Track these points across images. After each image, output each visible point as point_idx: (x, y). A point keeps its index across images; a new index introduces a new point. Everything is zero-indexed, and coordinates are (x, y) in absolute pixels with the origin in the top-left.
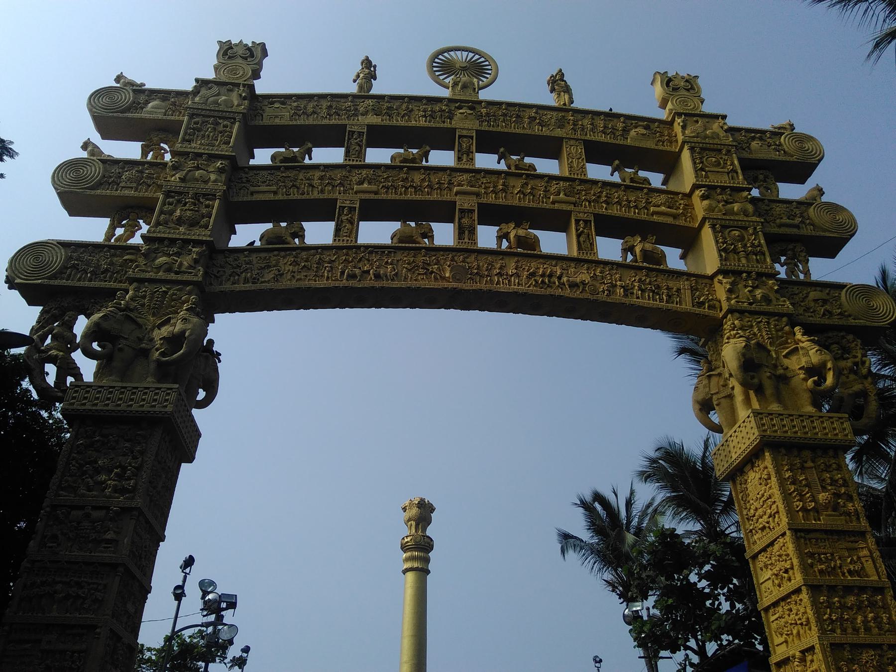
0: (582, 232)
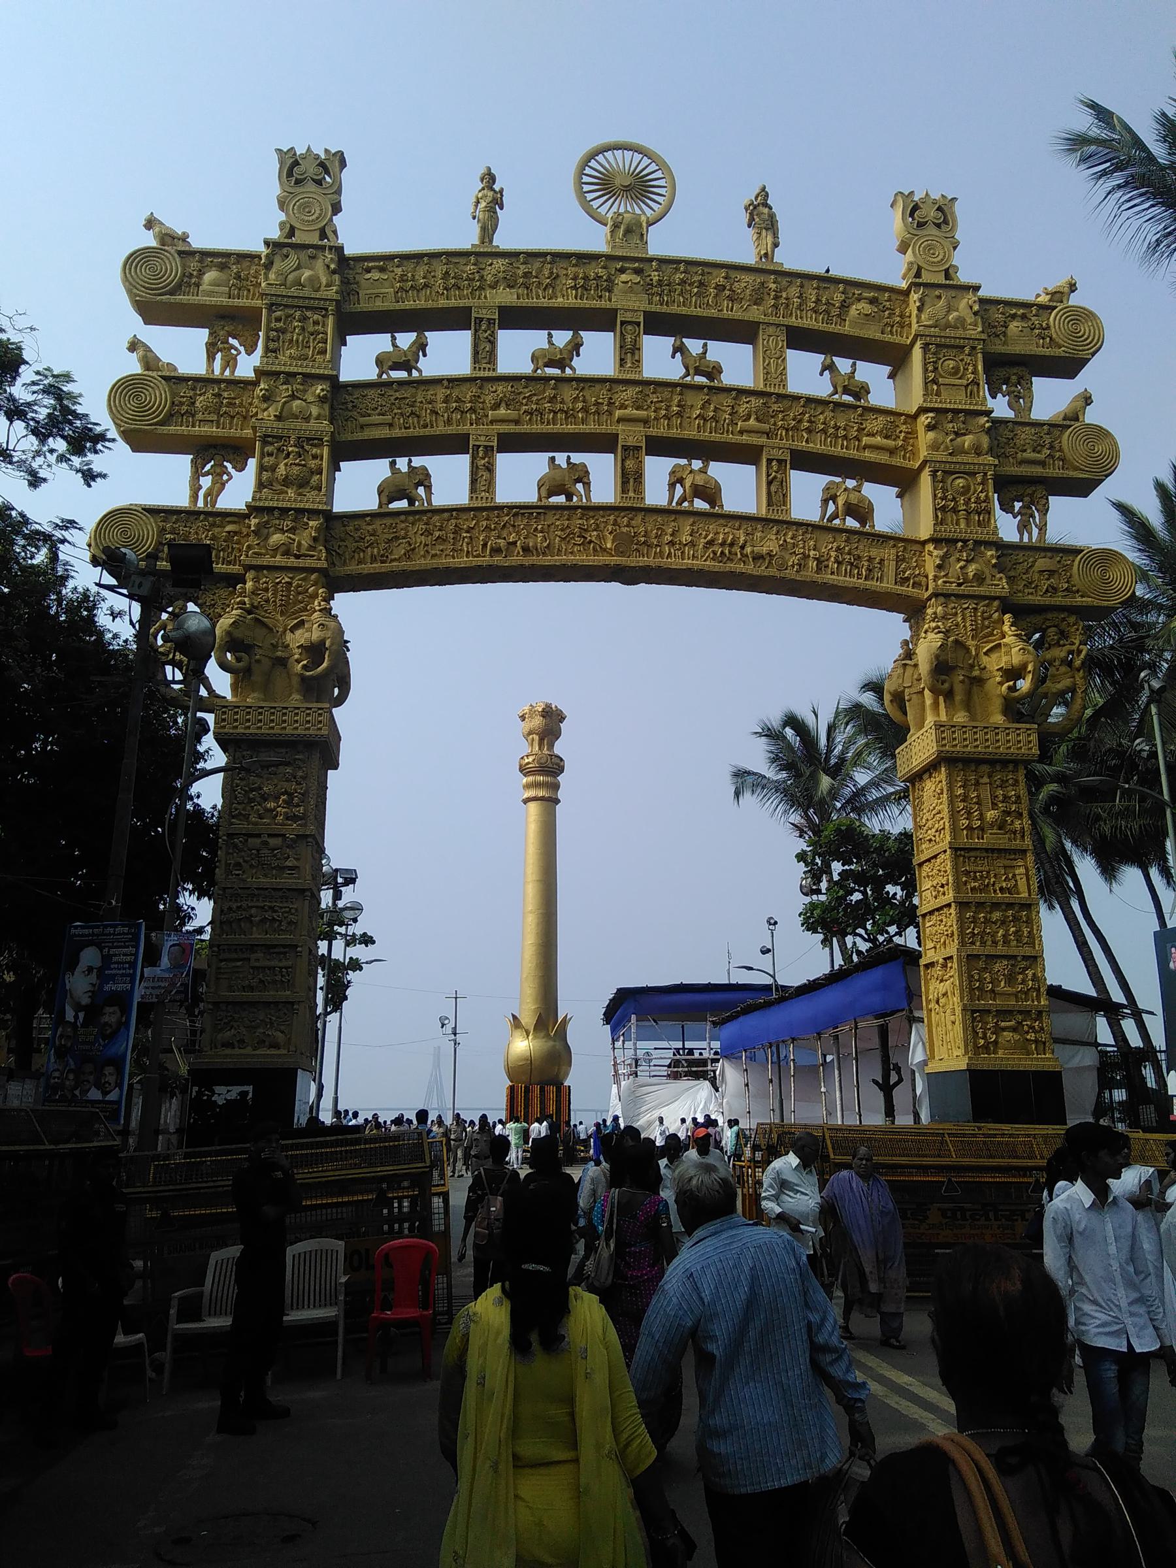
0: (775, 477)
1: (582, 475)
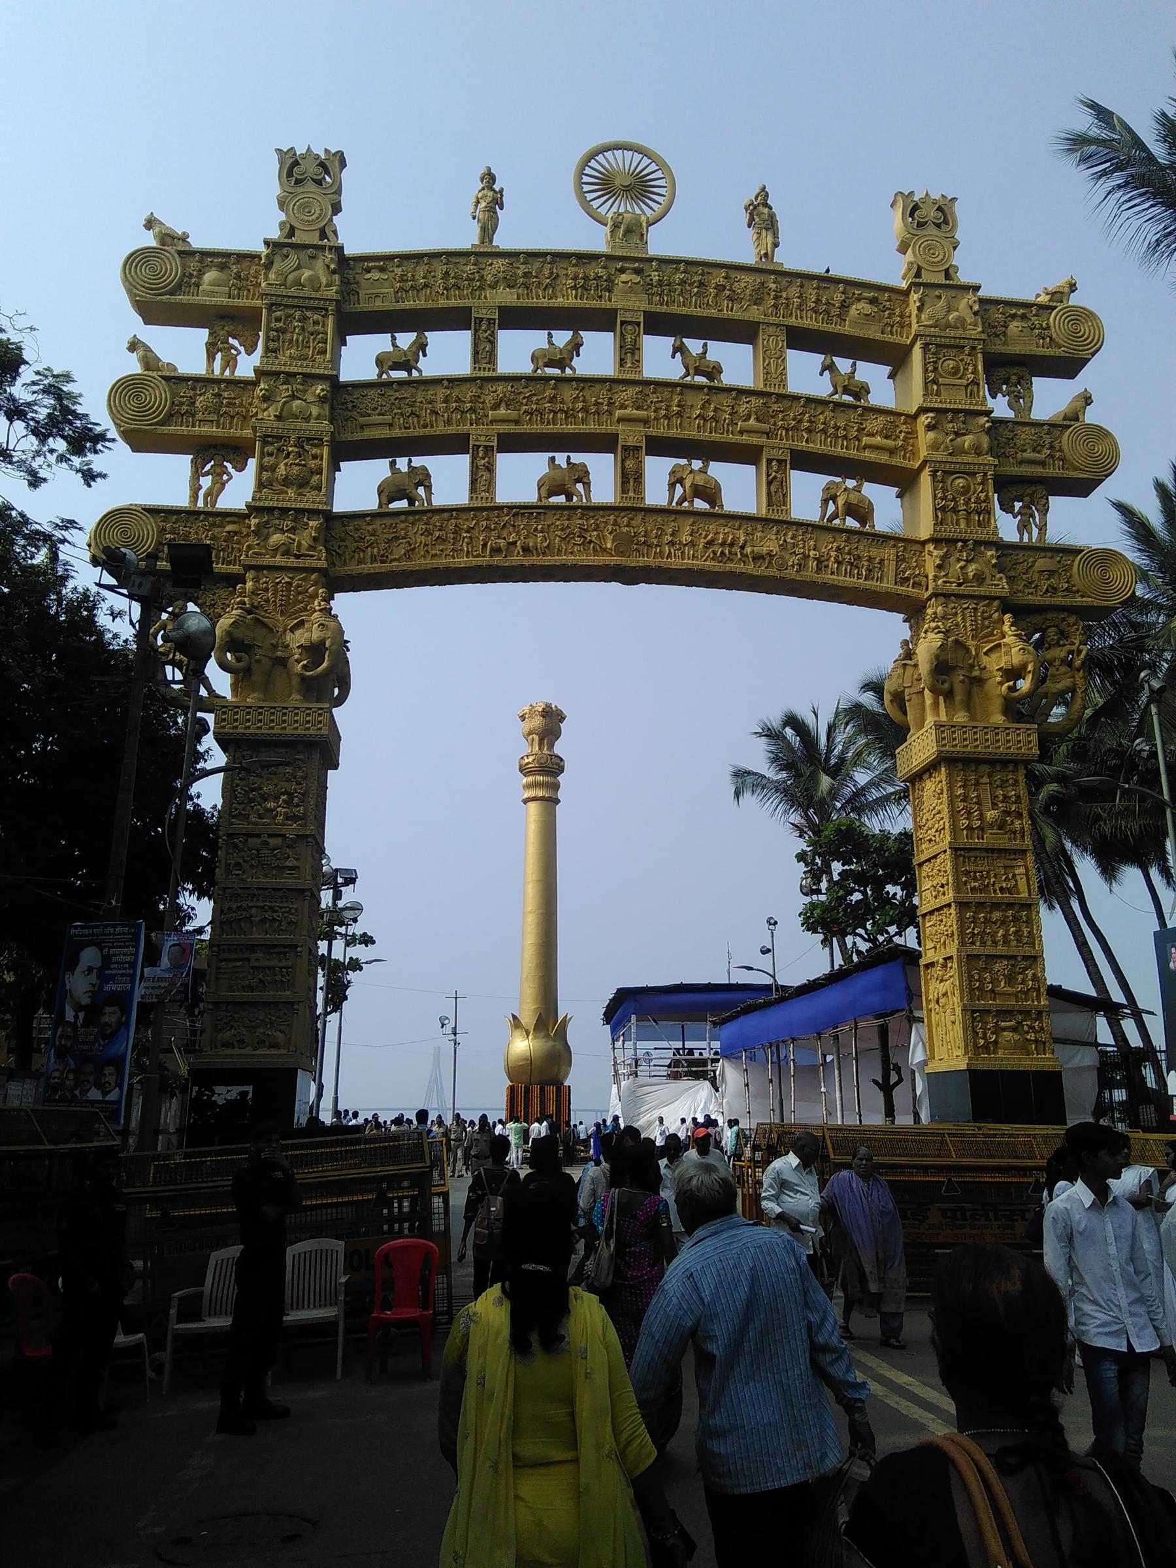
0: (775, 477)
1: (582, 475)
